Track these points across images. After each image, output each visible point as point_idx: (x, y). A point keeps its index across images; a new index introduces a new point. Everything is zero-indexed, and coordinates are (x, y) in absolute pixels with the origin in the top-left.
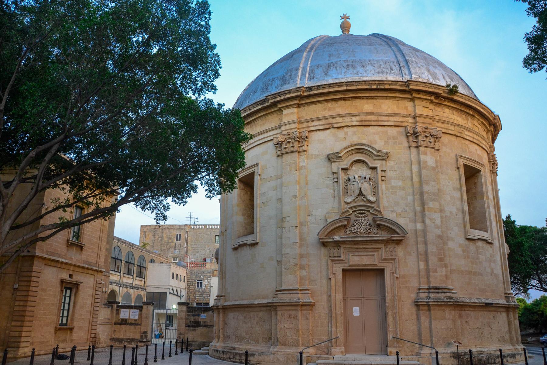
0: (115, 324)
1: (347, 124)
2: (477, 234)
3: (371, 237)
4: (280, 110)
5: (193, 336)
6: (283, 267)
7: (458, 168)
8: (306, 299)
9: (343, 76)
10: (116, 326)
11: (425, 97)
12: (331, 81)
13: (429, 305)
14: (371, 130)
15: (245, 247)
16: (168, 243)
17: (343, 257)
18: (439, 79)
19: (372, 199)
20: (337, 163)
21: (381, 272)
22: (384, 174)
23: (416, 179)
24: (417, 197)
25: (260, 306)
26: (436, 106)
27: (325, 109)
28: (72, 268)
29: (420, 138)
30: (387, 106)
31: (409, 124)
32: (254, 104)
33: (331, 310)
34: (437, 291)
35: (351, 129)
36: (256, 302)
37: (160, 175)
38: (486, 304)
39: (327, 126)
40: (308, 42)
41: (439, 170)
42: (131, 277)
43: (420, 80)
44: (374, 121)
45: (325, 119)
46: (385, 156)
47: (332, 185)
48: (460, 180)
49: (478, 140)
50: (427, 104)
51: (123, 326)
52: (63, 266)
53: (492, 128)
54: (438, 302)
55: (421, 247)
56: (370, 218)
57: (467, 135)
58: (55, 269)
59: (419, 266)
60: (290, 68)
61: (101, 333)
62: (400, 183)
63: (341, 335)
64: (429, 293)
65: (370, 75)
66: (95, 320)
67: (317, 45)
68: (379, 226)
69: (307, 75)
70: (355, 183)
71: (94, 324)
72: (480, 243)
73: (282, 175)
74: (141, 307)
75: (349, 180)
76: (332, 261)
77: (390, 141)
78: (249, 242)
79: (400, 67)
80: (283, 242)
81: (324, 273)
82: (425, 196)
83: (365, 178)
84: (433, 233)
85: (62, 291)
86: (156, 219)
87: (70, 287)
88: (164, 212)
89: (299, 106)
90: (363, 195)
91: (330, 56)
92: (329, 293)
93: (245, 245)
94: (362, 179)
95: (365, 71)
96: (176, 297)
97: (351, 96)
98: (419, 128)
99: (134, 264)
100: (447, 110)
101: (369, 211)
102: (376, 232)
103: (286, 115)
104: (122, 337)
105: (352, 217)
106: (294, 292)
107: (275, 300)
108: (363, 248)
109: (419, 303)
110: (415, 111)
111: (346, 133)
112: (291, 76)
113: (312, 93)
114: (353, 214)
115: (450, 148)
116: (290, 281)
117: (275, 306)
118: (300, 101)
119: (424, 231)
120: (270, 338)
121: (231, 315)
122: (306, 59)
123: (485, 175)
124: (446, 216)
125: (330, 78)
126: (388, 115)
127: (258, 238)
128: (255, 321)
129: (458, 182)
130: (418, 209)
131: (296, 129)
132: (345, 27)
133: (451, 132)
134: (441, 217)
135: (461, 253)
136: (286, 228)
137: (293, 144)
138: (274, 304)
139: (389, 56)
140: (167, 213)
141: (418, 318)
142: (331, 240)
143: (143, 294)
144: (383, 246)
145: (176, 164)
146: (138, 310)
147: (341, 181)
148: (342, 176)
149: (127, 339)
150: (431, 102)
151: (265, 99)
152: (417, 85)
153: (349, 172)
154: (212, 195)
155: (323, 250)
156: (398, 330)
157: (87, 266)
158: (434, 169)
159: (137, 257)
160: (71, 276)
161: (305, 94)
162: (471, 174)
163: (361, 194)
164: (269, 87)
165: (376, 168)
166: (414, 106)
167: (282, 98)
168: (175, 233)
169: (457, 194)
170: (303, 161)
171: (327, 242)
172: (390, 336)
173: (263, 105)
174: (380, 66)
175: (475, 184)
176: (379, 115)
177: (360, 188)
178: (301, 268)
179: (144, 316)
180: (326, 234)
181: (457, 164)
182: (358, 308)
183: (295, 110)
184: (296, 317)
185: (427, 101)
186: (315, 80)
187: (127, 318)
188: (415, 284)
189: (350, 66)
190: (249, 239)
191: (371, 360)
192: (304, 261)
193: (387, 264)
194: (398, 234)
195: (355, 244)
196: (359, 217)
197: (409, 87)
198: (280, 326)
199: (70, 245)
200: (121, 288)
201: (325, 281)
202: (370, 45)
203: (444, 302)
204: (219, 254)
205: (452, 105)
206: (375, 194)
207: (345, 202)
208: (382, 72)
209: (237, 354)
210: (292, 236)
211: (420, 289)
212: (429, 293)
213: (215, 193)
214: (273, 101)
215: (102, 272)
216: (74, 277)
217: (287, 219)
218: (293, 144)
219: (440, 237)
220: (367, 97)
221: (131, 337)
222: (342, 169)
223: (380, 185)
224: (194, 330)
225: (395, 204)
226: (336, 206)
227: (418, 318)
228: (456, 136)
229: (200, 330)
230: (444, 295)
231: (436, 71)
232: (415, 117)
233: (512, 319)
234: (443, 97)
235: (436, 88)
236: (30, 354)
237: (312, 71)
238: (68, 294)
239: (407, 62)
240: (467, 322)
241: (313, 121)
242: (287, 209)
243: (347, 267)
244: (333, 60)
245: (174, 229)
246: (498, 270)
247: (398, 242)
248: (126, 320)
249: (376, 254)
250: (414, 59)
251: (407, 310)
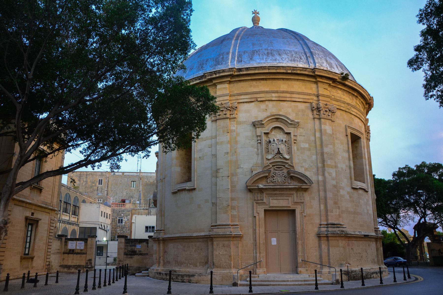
0: (64, 253)
1: (268, 99)
2: (359, 184)
3: (286, 185)
4: (215, 85)
5: (132, 262)
6: (218, 207)
7: (347, 135)
8: (235, 232)
9: (265, 62)
10: (65, 255)
11: (325, 81)
12: (255, 65)
13: (327, 237)
14: (284, 104)
15: (183, 192)
16: (92, 187)
17: (265, 201)
18: (334, 68)
19: (287, 157)
20: (260, 129)
21: (293, 212)
22: (295, 138)
23: (318, 143)
24: (319, 157)
25: (197, 238)
26: (332, 88)
27: (251, 86)
28: (34, 207)
29: (322, 112)
30: (297, 86)
31: (314, 101)
32: (193, 79)
33: (256, 240)
34: (333, 226)
35: (271, 102)
36: (195, 235)
37: (116, 133)
38: (365, 235)
40: (234, 31)
41: (335, 136)
42: (68, 215)
43: (322, 68)
44: (288, 97)
45: (251, 94)
46: (296, 125)
47: (256, 145)
48: (348, 144)
49: (359, 115)
50: (326, 86)
51: (71, 255)
52: (28, 206)
53: (367, 106)
54: (334, 234)
55: (322, 194)
56: (285, 171)
57: (353, 111)
58: (21, 208)
59: (320, 207)
60: (222, 52)
61: (53, 261)
62: (307, 146)
63: (263, 260)
64: (327, 227)
65: (285, 62)
66: (49, 250)
67: (241, 35)
68: (292, 178)
69: (236, 59)
70: (274, 144)
71: (49, 254)
72: (361, 192)
73: (216, 136)
74: (87, 240)
75: (270, 142)
76: (257, 203)
77: (300, 113)
78: (187, 188)
79: (307, 57)
80: (218, 188)
81: (250, 212)
82: (325, 156)
83: (282, 141)
84: (331, 182)
85: (26, 226)
86: (111, 168)
87: (32, 223)
88: (118, 163)
89: (230, 82)
90: (280, 154)
91: (253, 44)
92: (254, 228)
93: (184, 190)
94: (280, 141)
95: (282, 59)
96: (103, 231)
97: (271, 77)
98: (321, 104)
99: (70, 204)
100: (340, 92)
101: (284, 166)
102: (290, 181)
103: (219, 89)
104: (70, 264)
105: (272, 170)
106: (227, 227)
107: (211, 233)
108: (280, 194)
109: (321, 235)
110: (318, 91)
111: (267, 106)
112: (223, 58)
113: (241, 73)
114: (273, 168)
115: (342, 120)
116: (223, 219)
117: (212, 237)
118: (231, 79)
119: (324, 182)
120: (207, 263)
121: (170, 245)
122: (234, 46)
123: (363, 141)
124: (339, 171)
125: (254, 62)
126: (299, 93)
127: (195, 185)
128: (194, 250)
129: (347, 146)
130: (320, 165)
131: (228, 101)
132: (255, 20)
133: (342, 108)
134: (336, 171)
135: (348, 198)
136: (220, 178)
137: (226, 112)
138: (211, 236)
139: (298, 48)
140: (120, 164)
141: (320, 246)
142: (256, 187)
143: (77, 228)
144: (295, 193)
146: (83, 242)
147: (264, 143)
148: (264, 138)
149: (74, 266)
150: (330, 85)
151: (202, 76)
152: (320, 72)
153: (269, 136)
154: (167, 151)
155: (249, 195)
156: (306, 255)
157: (44, 206)
158: (331, 135)
159: (72, 199)
160: (33, 214)
161: (236, 74)
162: (355, 139)
163: (279, 153)
164: (204, 66)
165: (289, 133)
166: (318, 87)
167: (218, 75)
168: (98, 178)
169: (346, 155)
170: (233, 126)
171: (252, 189)
172: (300, 260)
173: (201, 80)
174: (292, 56)
176: (292, 93)
177: (279, 149)
178: (232, 209)
179: (89, 246)
180: (252, 182)
181: (346, 132)
182: (275, 239)
183: (227, 85)
184: (229, 246)
185: (327, 85)
187: (74, 248)
188: (317, 221)
189: (270, 54)
190: (188, 186)
191: (287, 277)
192: (235, 203)
193: (298, 206)
194: (306, 184)
195: (274, 191)
196: (277, 170)
197: (314, 73)
198: (216, 253)
199: (33, 188)
200: (61, 224)
201: (251, 219)
202: (283, 38)
203: (338, 234)
204: (158, 196)
205: (343, 88)
206: (289, 153)
207: (267, 159)
208: (294, 60)
209: (179, 275)
210: (224, 183)
211: (321, 225)
212: (327, 227)
213: (170, 149)
214: (210, 77)
215: (55, 210)
216: (35, 214)
217: (221, 170)
218: (226, 112)
219: (335, 186)
220: (283, 79)
221: (77, 264)
222: (265, 133)
223: (293, 147)
224: (131, 258)
225: (303, 162)
226: (259, 161)
227: (320, 246)
228: (346, 111)
229: (136, 257)
230: (338, 229)
231: (332, 62)
232: (318, 96)
233: (379, 247)
234: (338, 82)
235: (334, 75)
236: (5, 278)
237: (240, 56)
238: (30, 229)
239: (311, 53)
240: (352, 249)
241: (241, 95)
242: (221, 162)
243: (267, 208)
244: (256, 48)
245: (96, 175)
246: (371, 212)
247: (306, 190)
248: (73, 250)
249: (290, 198)
250: (316, 52)
251: (311, 240)
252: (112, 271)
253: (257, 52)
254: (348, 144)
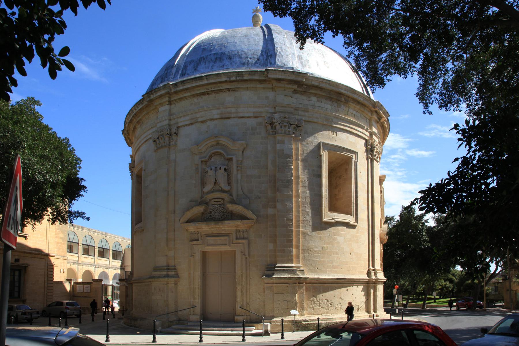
26: (301, 94)
39: (193, 121)
175: (346, 170)
186: (186, 75)
200: (97, 269)
252: (51, 300)
253: (204, 59)
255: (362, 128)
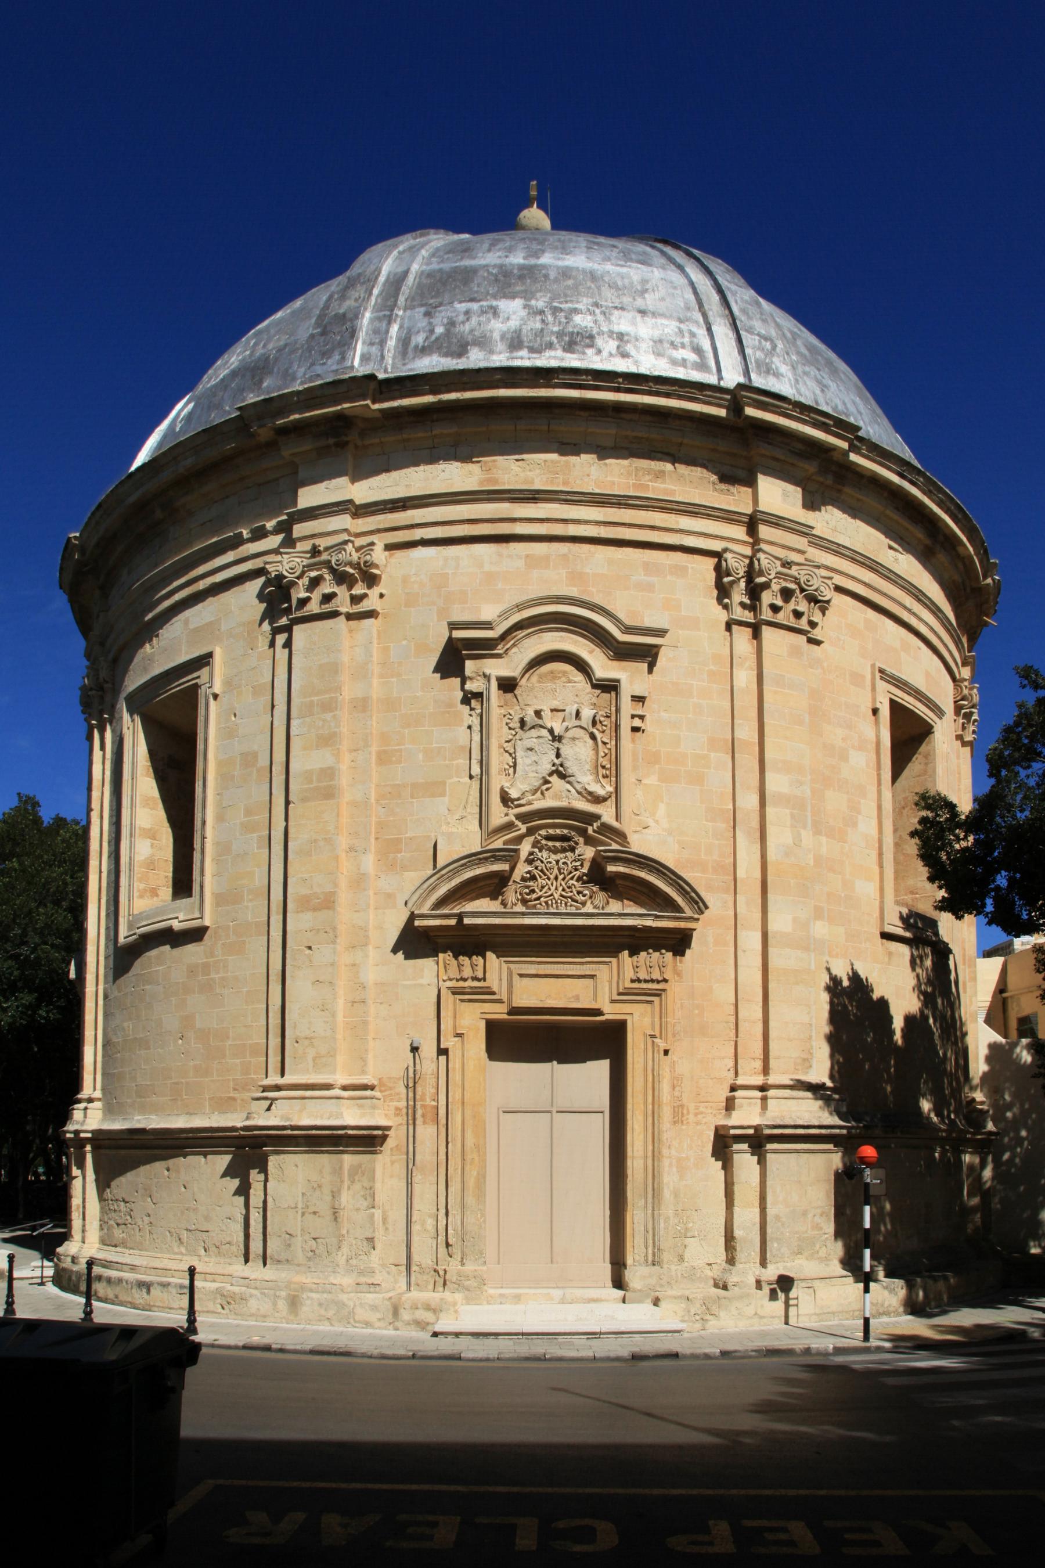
145: (916, 922)
194: (678, 909)
211: (733, 1089)
232: (752, 523)
254: (797, 1151)
255: (237, 542)
